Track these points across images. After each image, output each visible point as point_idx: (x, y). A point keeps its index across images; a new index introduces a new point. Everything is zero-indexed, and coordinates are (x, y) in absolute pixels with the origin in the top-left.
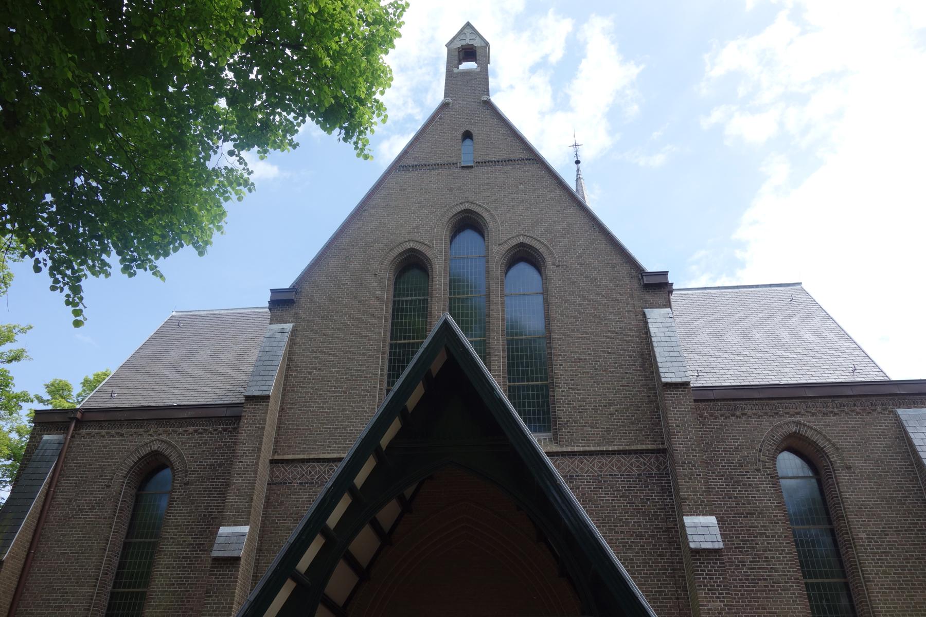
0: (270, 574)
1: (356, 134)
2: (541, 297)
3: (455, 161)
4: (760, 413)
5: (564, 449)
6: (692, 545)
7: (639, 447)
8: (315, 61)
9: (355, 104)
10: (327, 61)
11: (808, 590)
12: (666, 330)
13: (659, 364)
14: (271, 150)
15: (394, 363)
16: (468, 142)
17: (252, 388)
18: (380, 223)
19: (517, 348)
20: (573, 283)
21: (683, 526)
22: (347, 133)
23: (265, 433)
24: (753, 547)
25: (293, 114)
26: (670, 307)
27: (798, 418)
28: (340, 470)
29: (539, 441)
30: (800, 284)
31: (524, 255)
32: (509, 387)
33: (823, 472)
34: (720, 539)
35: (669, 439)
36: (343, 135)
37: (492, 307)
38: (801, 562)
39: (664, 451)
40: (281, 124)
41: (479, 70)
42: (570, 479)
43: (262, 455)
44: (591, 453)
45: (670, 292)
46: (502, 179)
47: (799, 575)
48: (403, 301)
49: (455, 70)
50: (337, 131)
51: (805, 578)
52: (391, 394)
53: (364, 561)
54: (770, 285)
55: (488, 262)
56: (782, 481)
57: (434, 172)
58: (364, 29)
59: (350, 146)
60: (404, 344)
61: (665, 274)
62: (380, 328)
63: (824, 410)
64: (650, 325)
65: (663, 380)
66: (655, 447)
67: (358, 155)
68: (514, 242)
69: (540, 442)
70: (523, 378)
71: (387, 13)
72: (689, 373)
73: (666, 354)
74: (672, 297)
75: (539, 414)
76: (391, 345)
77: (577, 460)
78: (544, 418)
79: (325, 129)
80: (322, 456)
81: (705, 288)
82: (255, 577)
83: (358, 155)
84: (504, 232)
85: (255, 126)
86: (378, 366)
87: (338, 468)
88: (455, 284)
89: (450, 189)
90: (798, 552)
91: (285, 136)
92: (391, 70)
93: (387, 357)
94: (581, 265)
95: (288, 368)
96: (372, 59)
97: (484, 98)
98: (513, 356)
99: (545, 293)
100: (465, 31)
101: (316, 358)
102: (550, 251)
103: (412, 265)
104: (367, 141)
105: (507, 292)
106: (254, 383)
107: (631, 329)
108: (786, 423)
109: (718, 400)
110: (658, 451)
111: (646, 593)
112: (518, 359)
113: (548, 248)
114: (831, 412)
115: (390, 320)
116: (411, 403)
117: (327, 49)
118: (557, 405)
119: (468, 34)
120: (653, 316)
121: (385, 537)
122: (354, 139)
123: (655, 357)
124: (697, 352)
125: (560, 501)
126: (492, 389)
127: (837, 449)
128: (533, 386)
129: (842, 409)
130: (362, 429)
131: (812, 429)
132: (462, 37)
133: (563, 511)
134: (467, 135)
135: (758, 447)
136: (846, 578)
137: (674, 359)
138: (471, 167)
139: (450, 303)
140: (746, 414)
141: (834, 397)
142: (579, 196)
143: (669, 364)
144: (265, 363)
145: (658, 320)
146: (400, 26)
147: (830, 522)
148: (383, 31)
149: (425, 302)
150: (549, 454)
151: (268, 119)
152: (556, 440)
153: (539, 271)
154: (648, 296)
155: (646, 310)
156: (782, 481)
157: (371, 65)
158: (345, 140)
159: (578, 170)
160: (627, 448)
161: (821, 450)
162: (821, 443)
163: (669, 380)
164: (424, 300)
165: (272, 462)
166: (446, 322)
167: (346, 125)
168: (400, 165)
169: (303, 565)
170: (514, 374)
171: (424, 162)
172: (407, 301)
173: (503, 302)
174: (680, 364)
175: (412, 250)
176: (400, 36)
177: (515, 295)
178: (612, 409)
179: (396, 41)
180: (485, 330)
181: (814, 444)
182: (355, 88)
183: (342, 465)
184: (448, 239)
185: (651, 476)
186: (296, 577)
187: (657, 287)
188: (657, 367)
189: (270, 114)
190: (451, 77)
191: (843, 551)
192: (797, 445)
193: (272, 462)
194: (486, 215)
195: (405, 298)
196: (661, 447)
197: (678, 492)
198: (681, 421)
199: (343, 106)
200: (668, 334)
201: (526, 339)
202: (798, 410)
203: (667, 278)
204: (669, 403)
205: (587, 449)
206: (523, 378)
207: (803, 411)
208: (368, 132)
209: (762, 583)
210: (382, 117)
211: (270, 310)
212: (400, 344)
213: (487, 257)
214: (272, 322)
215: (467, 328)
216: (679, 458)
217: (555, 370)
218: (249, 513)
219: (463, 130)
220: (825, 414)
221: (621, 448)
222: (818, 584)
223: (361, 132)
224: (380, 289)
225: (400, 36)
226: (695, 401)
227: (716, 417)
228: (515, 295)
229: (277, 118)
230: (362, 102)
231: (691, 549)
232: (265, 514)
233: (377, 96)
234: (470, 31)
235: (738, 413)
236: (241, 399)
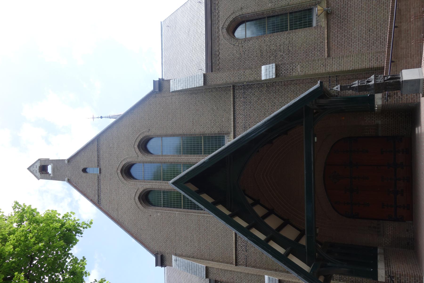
0: (286, 267)
1: (79, 228)
2: (163, 138)
3: (97, 177)
4: (218, 44)
5: (232, 130)
6: (274, 77)
7: (232, 97)
8: (40, 251)
9: (64, 229)
10: (41, 245)
11: (293, 29)
12: (180, 83)
13: (195, 86)
14: (86, 270)
15: (192, 207)
16: (88, 170)
17: (202, 275)
18: (126, 213)
19: (187, 150)
20: (157, 123)
21: (265, 80)
22: (79, 233)
23: (223, 268)
24: (275, 51)
25: (67, 260)
26: (170, 80)
27: (220, 28)
28: (240, 233)
29: (229, 141)
30: (161, 22)
31: (143, 146)
32: (204, 154)
33: (243, 19)
34: (271, 65)
35: (228, 84)
36: (79, 235)
37: (167, 161)
38: (281, 31)
39: (234, 86)
40: (72, 265)
41: (52, 164)
42: (245, 128)
43: (233, 270)
44: (234, 118)
45: (163, 79)
46: (107, 155)
47: (286, 32)
48: (163, 203)
49: (52, 175)
50: (77, 237)
51: (287, 30)
52: (206, 209)
53: (280, 222)
54: (162, 35)
55: (146, 162)
56: (247, 37)
57: (102, 187)
58: (25, 223)
59: (85, 231)
60: (183, 202)
61: (154, 81)
62: (175, 214)
63: (217, 16)
64: (178, 89)
65: (202, 85)
66: (232, 90)
67: (90, 227)
68: (137, 150)
69: (229, 141)
70: (180, 200)
71: (18, 212)
72: (200, 73)
73: (191, 83)
74: (165, 79)
75: (217, 141)
76: (184, 208)
77: (237, 125)
78: (218, 139)
79: (76, 243)
80: (234, 241)
81: (162, 64)
82: (288, 272)
83: (90, 227)
84: (132, 154)
85: (73, 278)
86: (193, 214)
87: (239, 234)
88: (156, 177)
89: (110, 179)
90: (277, 32)
91: (79, 264)
92: (48, 210)
93: (189, 210)
94: (149, 119)
95: (193, 257)
96: (41, 220)
97: (66, 162)
98: (190, 152)
99: (161, 136)
100: (32, 171)
101: (189, 244)
102: (142, 133)
103: (146, 198)
104: (83, 222)
105: (160, 154)
106: (200, 274)
107: (179, 98)
108: (222, 34)
109: (212, 62)
110: (234, 89)
111: (294, 97)
112: (192, 150)
113: (141, 134)
114: (218, 14)
115: (172, 209)
116: (210, 200)
117: (35, 244)
118: (212, 133)
119: (34, 169)
120: (173, 88)
121: (271, 212)
122: (81, 229)
123: (192, 88)
124: (190, 69)
125: (254, 134)
126: (204, 163)
127: (234, 12)
128: (204, 143)
129: (216, 9)
130: (222, 223)
131: (225, 23)
132: (35, 172)
133: (258, 133)
134: (84, 170)
135: (232, 46)
136: (287, 13)
137: (193, 80)
138: (100, 169)
139: (165, 180)
140: (218, 50)
141: (211, 12)
142: (118, 117)
143: (196, 82)
144: (191, 269)
145: (176, 86)
146: (25, 206)
147: (265, 18)
148: (25, 214)
149: (164, 192)
150: (234, 137)
151: (69, 272)
152: (228, 134)
153: (153, 138)
154: (164, 90)
155: (171, 91)
156: (247, 36)
157: (44, 220)
158: (82, 233)
159: (105, 117)
160: (232, 102)
161: (234, 20)
162: (231, 19)
163: (202, 83)
164: (163, 193)
165: (236, 265)
166: (174, 183)
167: (74, 233)
168: (97, 203)
169: (281, 250)
170: (198, 152)
171: (97, 192)
172: (163, 201)
173: (165, 156)
174: (195, 77)
175: (139, 198)
176: (30, 206)
177: (162, 150)
178: (215, 108)
179: (33, 207)
180: (178, 164)
181: (231, 22)
182: (56, 228)
183: (237, 232)
184: (135, 180)
185: (244, 93)
186: (287, 254)
187: (161, 86)
188: (197, 87)
189: (66, 271)
190: (55, 177)
191: (276, 14)
192: (232, 29)
193: (236, 265)
194: (124, 163)
195: (162, 199)
196: (232, 88)
197: (251, 82)
198: (221, 78)
199: (65, 234)
200: (182, 82)
201: (183, 146)
202: (217, 28)
203: (157, 81)
204: (213, 83)
205: (232, 120)
206: (180, 200)
207: (218, 26)
208: (78, 222)
209: (290, 48)
210: (72, 215)
211: (165, 266)
212: (183, 204)
213: (143, 162)
214: (171, 265)
215: (177, 173)
216: (237, 80)
217: (197, 133)
218: (259, 275)
219: (82, 173)
220: (219, 17)
221: (232, 105)
222: (290, 25)
223: (79, 226)
224: (157, 213)
225: (30, 206)
226: (212, 72)
227: (219, 63)
228: (162, 150)
229: (69, 267)
230: (63, 225)
231: (275, 77)
232: (259, 268)
233: (61, 217)
234: (32, 168)
235: (218, 53)
236: (207, 280)
